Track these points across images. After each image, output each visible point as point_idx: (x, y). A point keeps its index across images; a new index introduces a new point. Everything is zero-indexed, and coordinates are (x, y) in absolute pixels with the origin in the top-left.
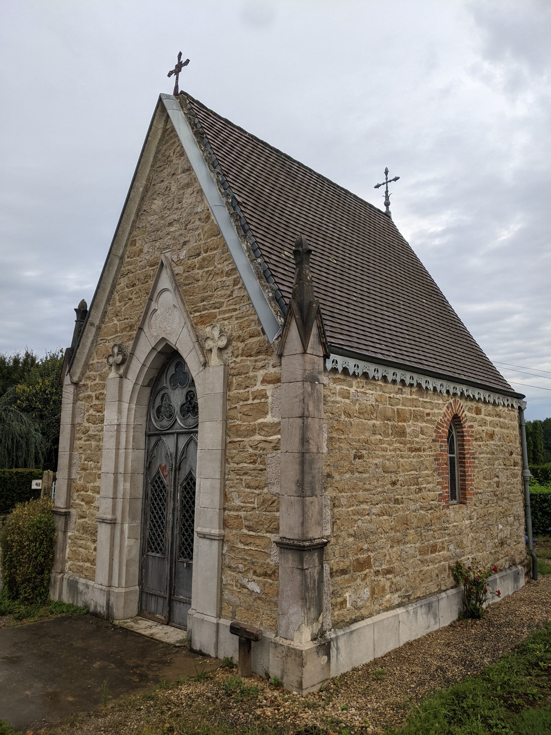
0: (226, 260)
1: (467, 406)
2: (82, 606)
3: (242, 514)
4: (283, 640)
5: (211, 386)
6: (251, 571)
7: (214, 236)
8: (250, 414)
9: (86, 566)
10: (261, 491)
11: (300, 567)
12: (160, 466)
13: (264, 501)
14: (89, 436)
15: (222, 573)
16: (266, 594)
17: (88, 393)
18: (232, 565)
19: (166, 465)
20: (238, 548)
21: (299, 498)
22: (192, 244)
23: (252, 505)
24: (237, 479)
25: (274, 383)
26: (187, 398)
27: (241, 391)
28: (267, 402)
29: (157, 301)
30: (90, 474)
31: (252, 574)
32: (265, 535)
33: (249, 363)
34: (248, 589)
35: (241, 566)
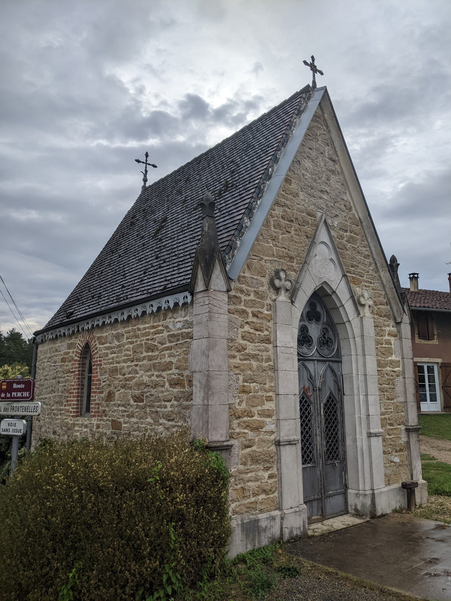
1: (177, 352)
9: (260, 500)
14: (248, 355)
17: (241, 307)
19: (309, 387)
23: (390, 410)
30: (254, 397)
34: (394, 462)
35: (181, 459)
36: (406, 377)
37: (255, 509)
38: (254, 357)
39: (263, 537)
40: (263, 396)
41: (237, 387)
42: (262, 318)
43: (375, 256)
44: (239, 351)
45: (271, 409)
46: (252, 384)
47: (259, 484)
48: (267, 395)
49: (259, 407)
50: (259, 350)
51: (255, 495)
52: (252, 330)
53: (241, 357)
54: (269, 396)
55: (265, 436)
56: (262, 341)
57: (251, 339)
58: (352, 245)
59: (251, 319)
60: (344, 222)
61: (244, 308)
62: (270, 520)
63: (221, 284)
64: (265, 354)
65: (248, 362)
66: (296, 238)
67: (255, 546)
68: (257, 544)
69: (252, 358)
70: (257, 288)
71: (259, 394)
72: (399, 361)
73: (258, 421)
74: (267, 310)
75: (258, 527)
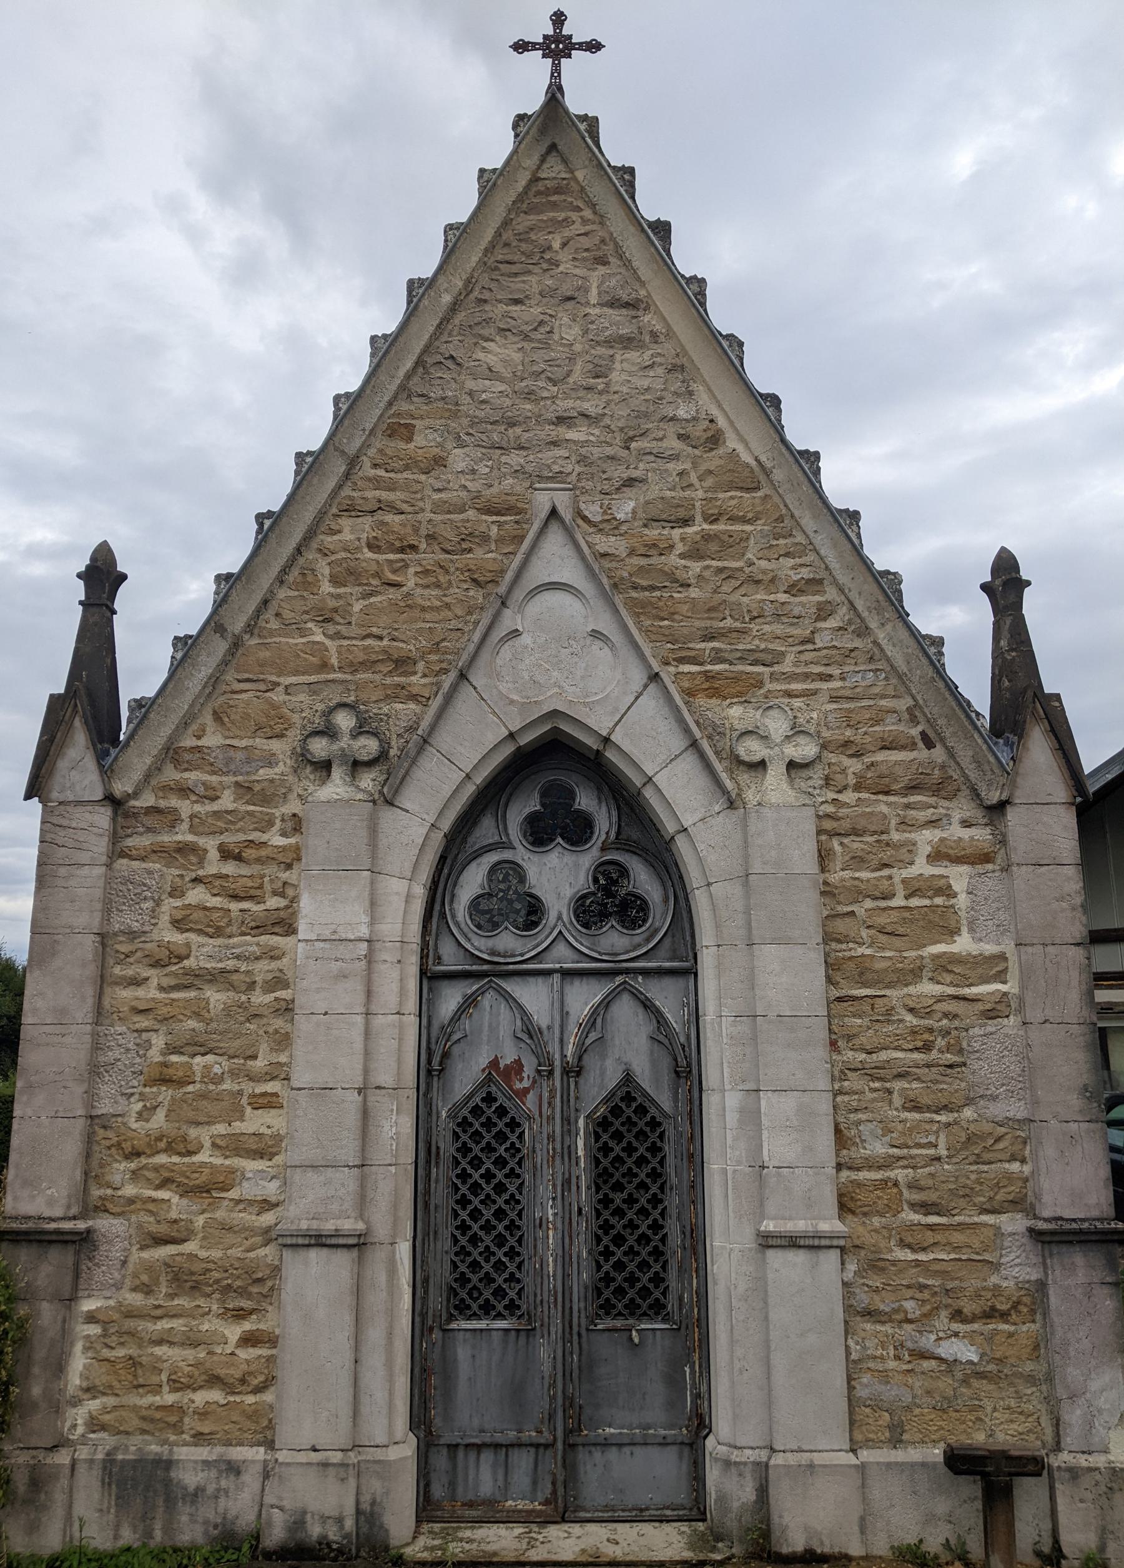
0: (787, 555)
2: (200, 1539)
3: (900, 1174)
4: (1086, 1456)
5: (773, 853)
6: (944, 1314)
7: (741, 489)
8: (901, 931)
10: (956, 1115)
11: (1109, 1279)
12: (494, 1063)
13: (969, 1139)
15: (847, 1332)
16: (1000, 1361)
17: (179, 838)
18: (882, 1307)
20: (894, 1263)
21: (1092, 1125)
22: (654, 490)
23: (932, 1152)
24: (876, 1090)
25: (973, 864)
26: (596, 880)
27: (864, 875)
28: (952, 906)
29: (521, 609)
30: (203, 1096)
31: (946, 1321)
32: (976, 1219)
33: (884, 809)
35: (909, 1305)
36: (360, 1019)
37: (177, 1428)
38: (219, 978)
39: (184, 1518)
40: (240, 1093)
41: (138, 1068)
42: (259, 861)
43: (842, 579)
44: (157, 964)
45: (269, 1132)
46: (198, 1059)
47: (202, 1355)
48: (257, 1091)
49: (218, 1126)
50: (238, 957)
51: (178, 1385)
52: (218, 899)
53: (166, 981)
54: (264, 1094)
55: (235, 1215)
56: (259, 928)
57: (209, 926)
58: (714, 563)
59: (213, 865)
60: (669, 494)
61: (190, 838)
62: (220, 1472)
63: (86, 782)
64: (263, 965)
65: (192, 994)
66: (423, 597)
67: (149, 1534)
68: (158, 1534)
69: (211, 981)
70: (248, 773)
71: (225, 1087)
72: (1002, 957)
73: (212, 1166)
74: (284, 834)
75: (168, 1483)
